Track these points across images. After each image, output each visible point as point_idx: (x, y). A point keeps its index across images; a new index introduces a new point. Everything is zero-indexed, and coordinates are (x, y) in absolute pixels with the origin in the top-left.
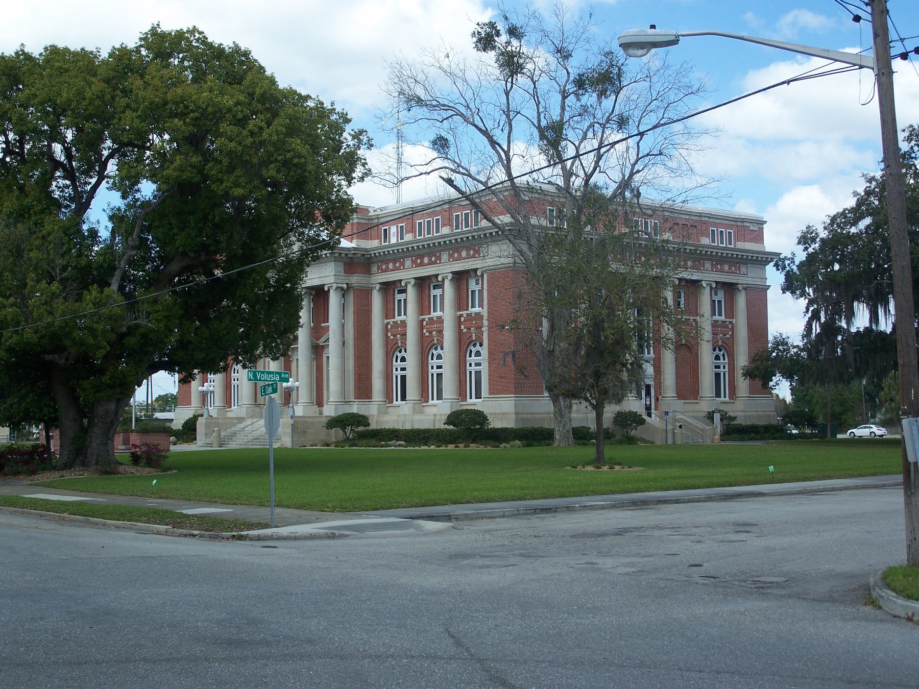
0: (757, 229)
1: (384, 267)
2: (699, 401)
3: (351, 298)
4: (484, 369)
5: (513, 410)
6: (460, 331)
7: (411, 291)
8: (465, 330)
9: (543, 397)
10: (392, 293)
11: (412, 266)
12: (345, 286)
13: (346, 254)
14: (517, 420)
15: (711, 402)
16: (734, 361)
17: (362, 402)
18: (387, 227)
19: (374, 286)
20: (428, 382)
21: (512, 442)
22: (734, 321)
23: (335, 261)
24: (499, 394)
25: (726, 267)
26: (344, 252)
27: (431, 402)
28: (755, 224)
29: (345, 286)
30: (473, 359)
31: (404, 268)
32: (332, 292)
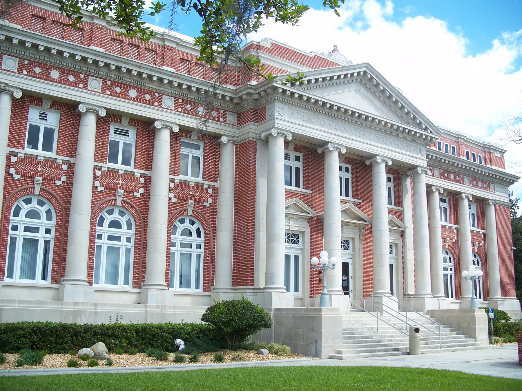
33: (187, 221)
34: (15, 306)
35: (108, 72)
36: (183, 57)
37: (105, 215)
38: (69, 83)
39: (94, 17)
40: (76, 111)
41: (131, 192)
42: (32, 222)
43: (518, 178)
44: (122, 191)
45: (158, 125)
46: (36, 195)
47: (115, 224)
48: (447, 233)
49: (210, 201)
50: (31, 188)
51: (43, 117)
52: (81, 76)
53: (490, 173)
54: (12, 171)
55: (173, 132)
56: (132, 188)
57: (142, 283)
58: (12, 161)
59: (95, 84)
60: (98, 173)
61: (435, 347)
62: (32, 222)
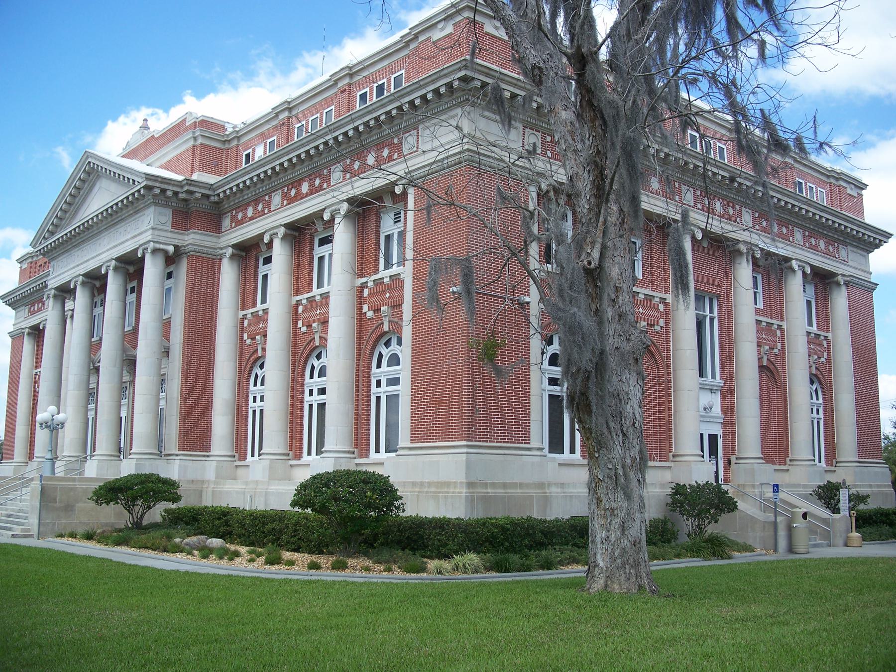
0: (856, 195)
1: (240, 216)
2: (790, 468)
3: (183, 270)
4: (404, 390)
5: (462, 478)
6: (361, 315)
7: (280, 252)
8: (370, 314)
9: (529, 449)
10: (253, 263)
11: (282, 203)
12: (171, 249)
13: (176, 194)
14: (471, 500)
15: (811, 469)
16: (832, 401)
17: (191, 455)
18: (250, 150)
19: (224, 251)
20: (302, 421)
21: (458, 558)
22: (830, 335)
23: (156, 204)
24: (438, 439)
26: (170, 188)
27: (306, 458)
28: (853, 187)
29: (171, 249)
30: (385, 371)
31: (270, 211)
32: (148, 257)
43: (888, 236)
44: (645, 324)
48: (764, 336)
49: (662, 322)
53: (835, 222)
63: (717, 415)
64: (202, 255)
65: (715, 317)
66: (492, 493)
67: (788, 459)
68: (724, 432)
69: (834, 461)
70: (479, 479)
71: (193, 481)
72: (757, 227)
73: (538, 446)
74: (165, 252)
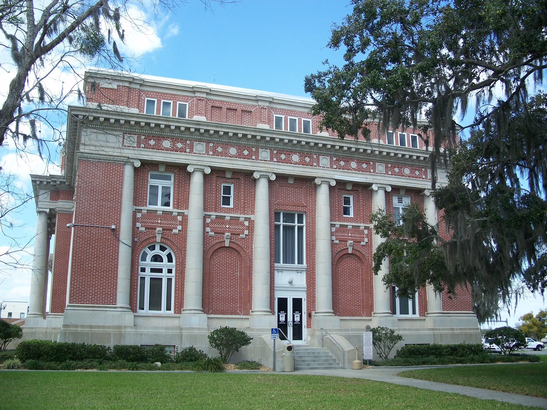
12: (48, 211)
14: (64, 334)
15: (384, 319)
25: (354, 165)
33: (157, 247)
34: (349, 334)
35: (140, 128)
36: (244, 109)
37: (147, 250)
38: (245, 157)
39: (196, 92)
40: (252, 177)
41: (169, 229)
42: (157, 265)
45: (374, 187)
46: (158, 242)
47: (157, 258)
48: (350, 235)
50: (223, 241)
51: (400, 201)
52: (14, 122)
54: (208, 229)
55: (331, 185)
56: (237, 231)
57: (250, 310)
58: (138, 217)
59: (264, 154)
60: (334, 229)
61: (309, 361)
62: (157, 265)
63: (303, 286)
64: (64, 212)
65: (304, 226)
66: (80, 330)
67: (372, 312)
68: (308, 296)
69: (250, 310)
70: (73, 323)
71: (55, 328)
72: (335, 166)
73: (120, 306)
74: (45, 212)
